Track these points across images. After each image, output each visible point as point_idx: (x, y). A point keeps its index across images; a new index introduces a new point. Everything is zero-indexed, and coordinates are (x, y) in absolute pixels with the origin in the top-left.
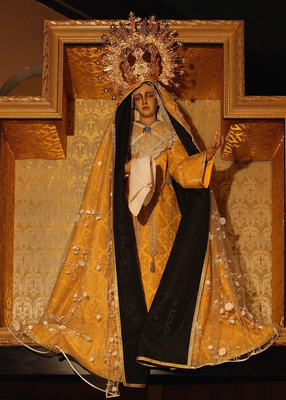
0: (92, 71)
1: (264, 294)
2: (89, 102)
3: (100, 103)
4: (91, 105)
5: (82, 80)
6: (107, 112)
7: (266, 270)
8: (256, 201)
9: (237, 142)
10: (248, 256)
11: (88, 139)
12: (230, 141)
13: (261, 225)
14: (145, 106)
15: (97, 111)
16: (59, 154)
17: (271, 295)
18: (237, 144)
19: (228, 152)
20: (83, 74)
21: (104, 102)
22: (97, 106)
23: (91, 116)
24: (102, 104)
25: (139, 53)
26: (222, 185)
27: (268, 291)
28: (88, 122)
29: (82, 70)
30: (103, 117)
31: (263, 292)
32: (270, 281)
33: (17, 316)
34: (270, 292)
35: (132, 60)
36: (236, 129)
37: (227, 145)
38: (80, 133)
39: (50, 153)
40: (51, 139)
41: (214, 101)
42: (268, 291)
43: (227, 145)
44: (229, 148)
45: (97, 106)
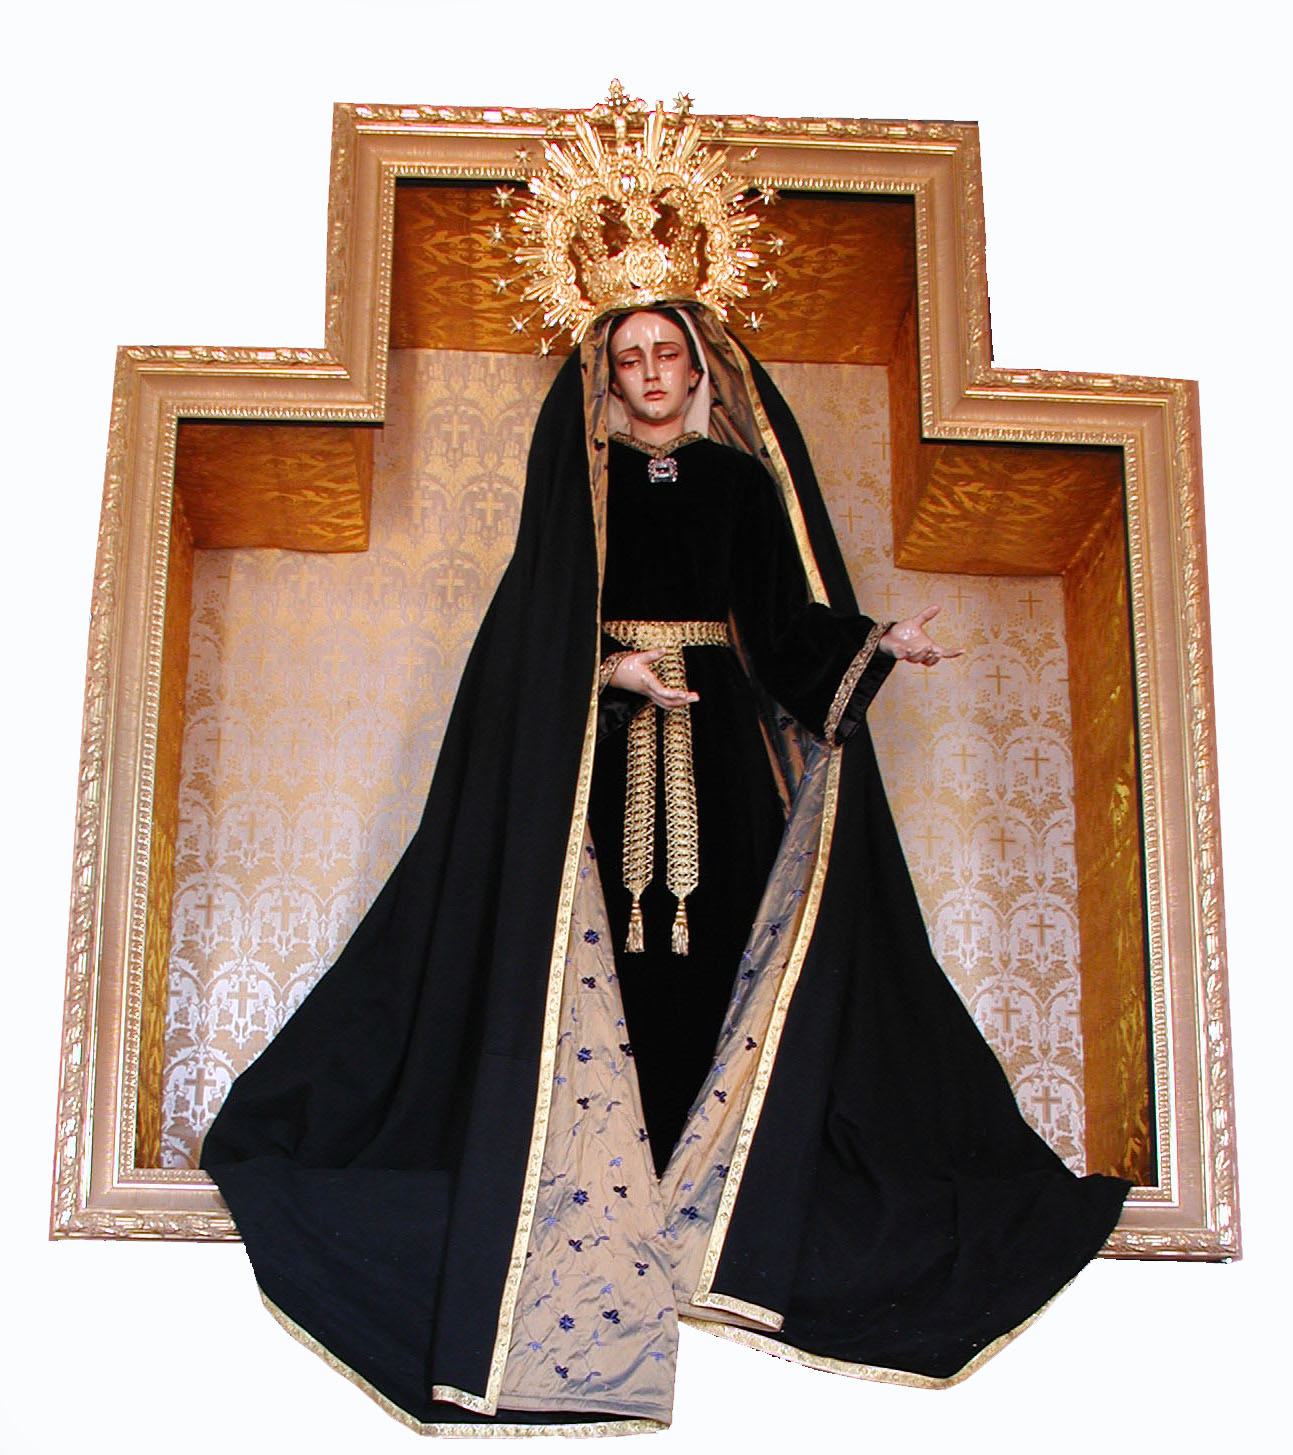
0: (475, 261)
1: (1058, 1052)
2: (447, 356)
3: (485, 363)
4: (457, 370)
5: (435, 290)
6: (508, 392)
7: (1060, 964)
8: (1016, 713)
9: (957, 513)
10: (1032, 828)
11: (443, 481)
12: (932, 508)
13: (1038, 800)
14: (650, 387)
15: (473, 392)
16: (347, 534)
17: (1081, 1057)
18: (956, 518)
19: (921, 542)
20: (444, 270)
21: (498, 360)
22: (477, 371)
23: (456, 407)
24: (492, 369)
25: (640, 216)
26: (293, 976)
27: (1068, 1044)
28: (445, 427)
29: (441, 257)
30: (496, 412)
31: (1054, 1045)
32: (1075, 1008)
33: (180, 1122)
34: (1078, 1045)
35: (615, 235)
36: (955, 470)
37: (921, 520)
38: (490, 465)
39: (317, 530)
40: (332, 485)
41: (868, 369)
42: (1071, 1044)
43: (921, 520)
44: (926, 530)
45: (477, 371)
